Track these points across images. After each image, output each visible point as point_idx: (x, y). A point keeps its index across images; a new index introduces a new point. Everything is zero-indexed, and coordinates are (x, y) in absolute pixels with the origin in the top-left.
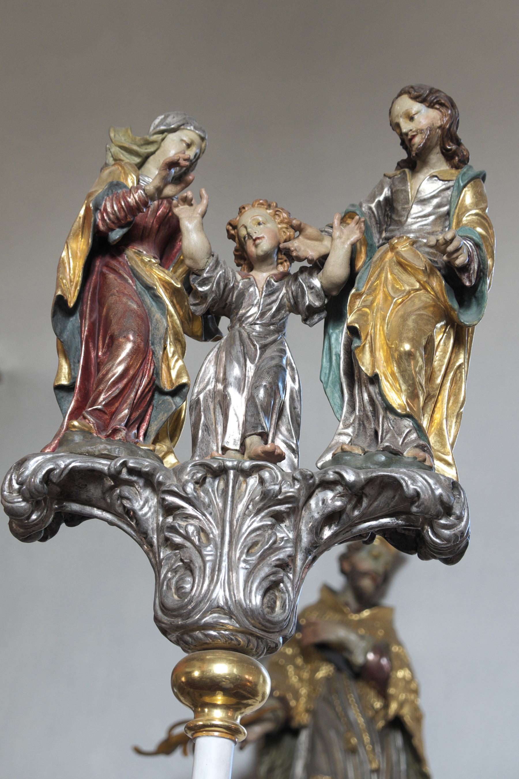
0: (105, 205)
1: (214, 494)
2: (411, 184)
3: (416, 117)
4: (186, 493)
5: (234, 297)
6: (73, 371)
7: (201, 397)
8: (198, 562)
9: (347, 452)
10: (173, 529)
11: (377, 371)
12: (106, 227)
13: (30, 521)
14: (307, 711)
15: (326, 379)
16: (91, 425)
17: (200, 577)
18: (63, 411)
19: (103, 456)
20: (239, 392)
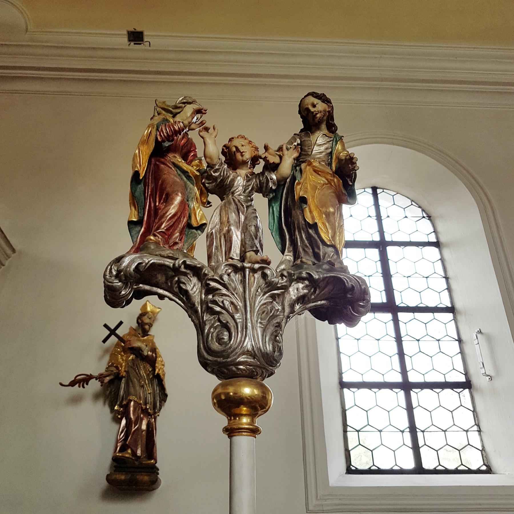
0: (162, 128)
1: (237, 282)
2: (312, 138)
3: (317, 105)
4: (223, 280)
5: (228, 181)
6: (140, 213)
7: (214, 231)
8: (232, 324)
9: (304, 263)
10: (215, 303)
11: (316, 221)
12: (161, 139)
13: (121, 294)
14: (125, 371)
15: (272, 228)
16: (160, 240)
17: (235, 332)
18: (132, 235)
19: (170, 257)
20: (237, 229)
